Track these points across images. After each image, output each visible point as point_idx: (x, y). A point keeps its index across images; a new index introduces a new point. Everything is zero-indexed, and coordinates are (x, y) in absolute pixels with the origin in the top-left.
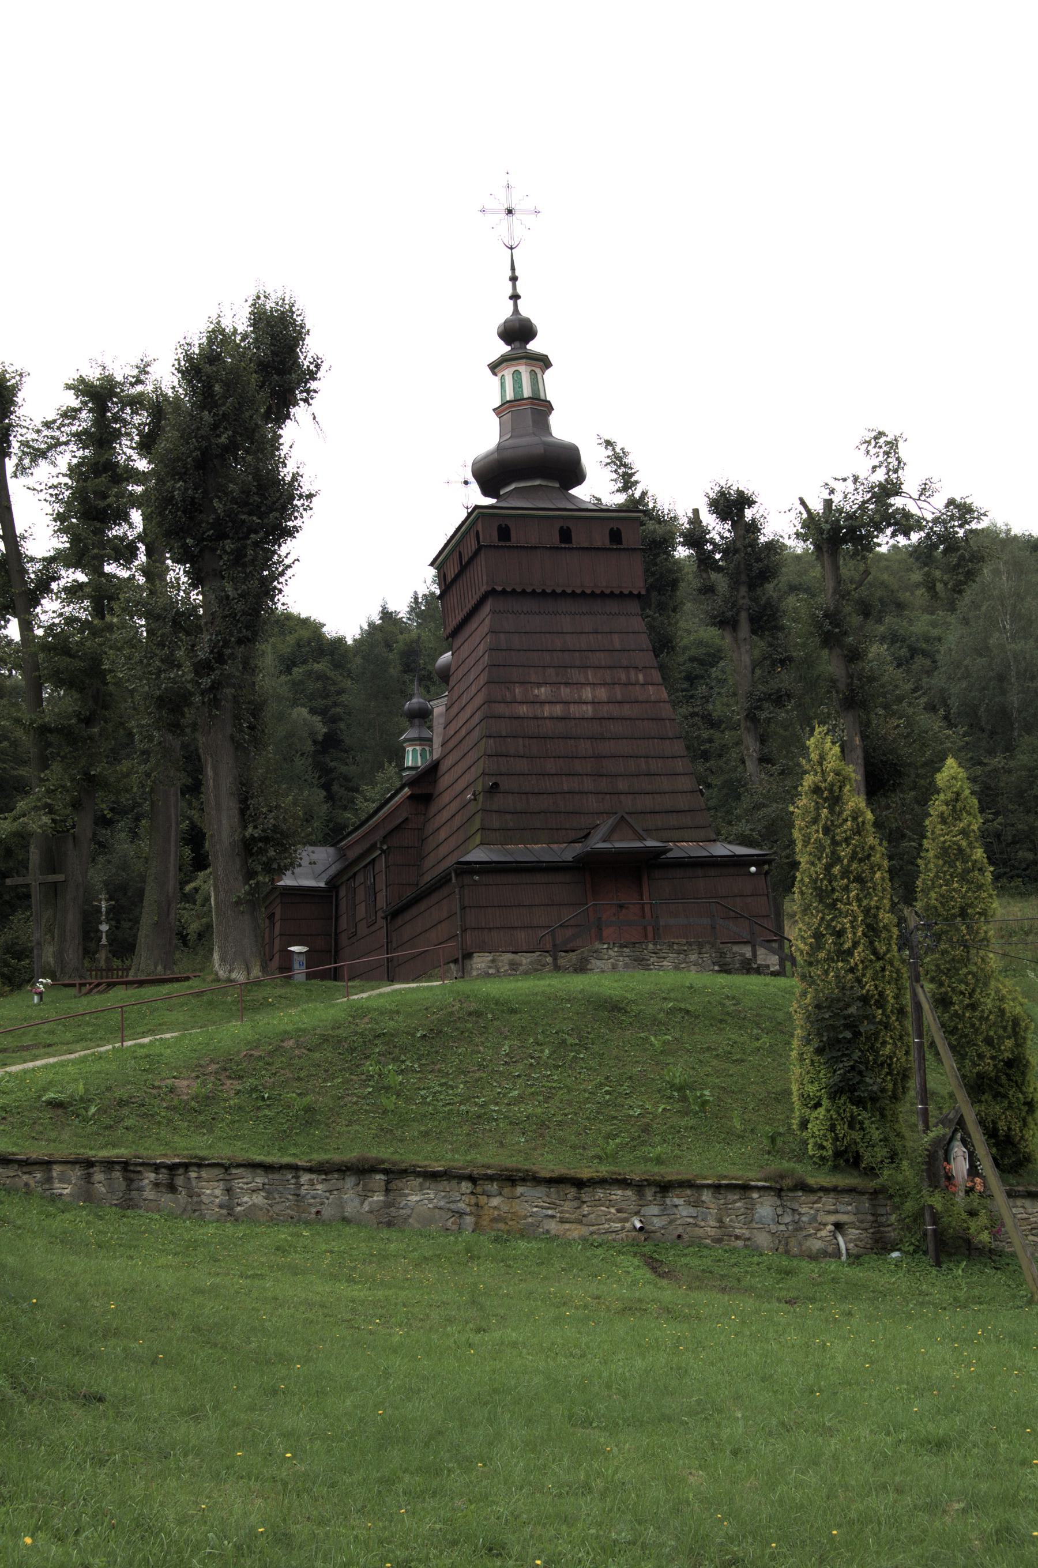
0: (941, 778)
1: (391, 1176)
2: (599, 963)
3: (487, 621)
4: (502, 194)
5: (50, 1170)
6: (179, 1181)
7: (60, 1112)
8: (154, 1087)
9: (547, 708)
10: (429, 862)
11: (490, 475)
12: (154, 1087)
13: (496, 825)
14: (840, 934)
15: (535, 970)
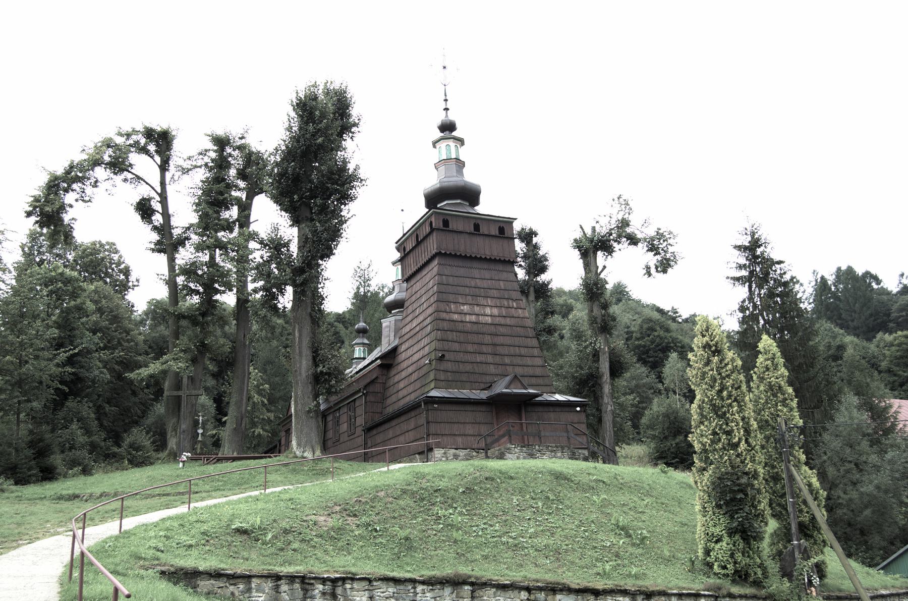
0: (761, 346)
1: (476, 587)
2: (510, 456)
3: (436, 269)
5: (250, 583)
6: (339, 591)
7: (245, 537)
8: (304, 521)
9: (468, 316)
10: (389, 401)
11: (433, 199)
12: (304, 521)
13: (442, 378)
14: (729, 433)
15: (468, 458)
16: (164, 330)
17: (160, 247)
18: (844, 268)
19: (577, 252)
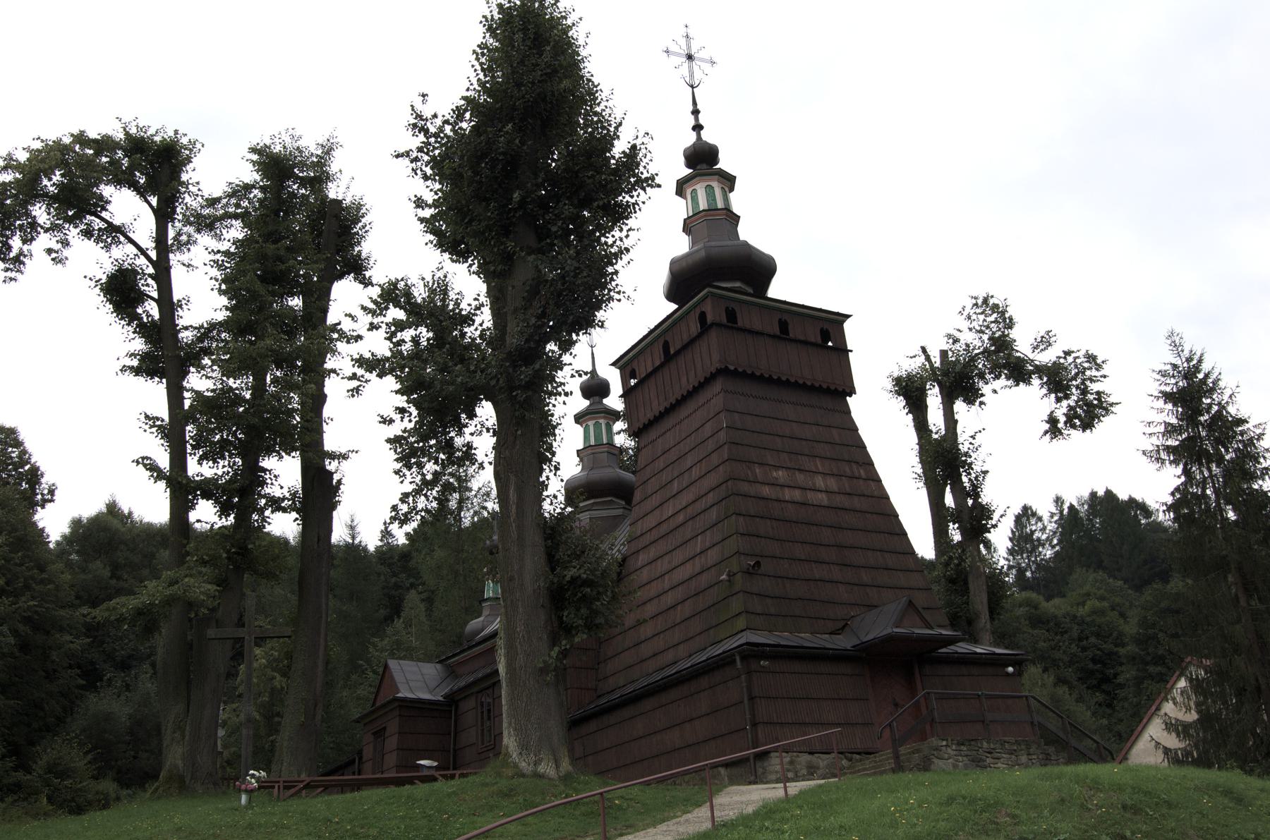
2: (941, 763)
4: (683, 42)
16: (100, 568)
17: (147, 367)
18: (1101, 493)
19: (901, 402)
